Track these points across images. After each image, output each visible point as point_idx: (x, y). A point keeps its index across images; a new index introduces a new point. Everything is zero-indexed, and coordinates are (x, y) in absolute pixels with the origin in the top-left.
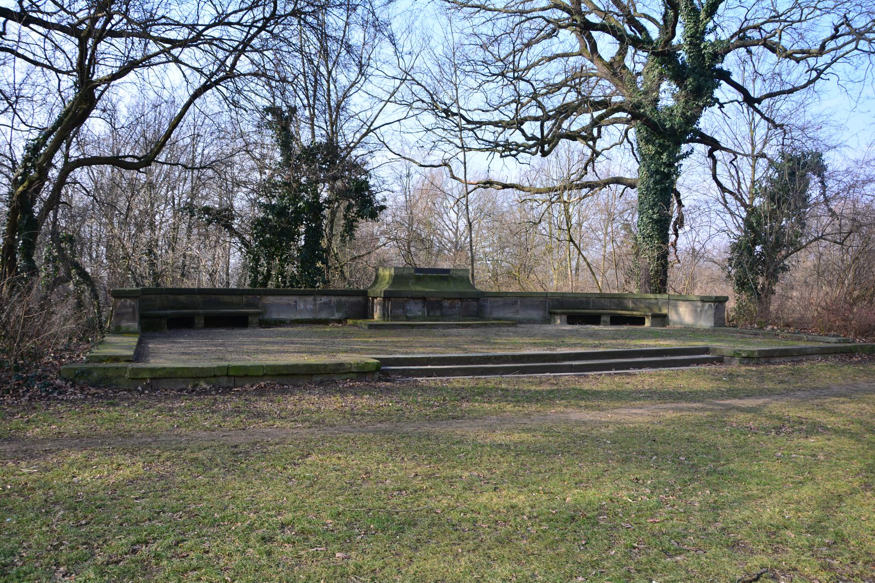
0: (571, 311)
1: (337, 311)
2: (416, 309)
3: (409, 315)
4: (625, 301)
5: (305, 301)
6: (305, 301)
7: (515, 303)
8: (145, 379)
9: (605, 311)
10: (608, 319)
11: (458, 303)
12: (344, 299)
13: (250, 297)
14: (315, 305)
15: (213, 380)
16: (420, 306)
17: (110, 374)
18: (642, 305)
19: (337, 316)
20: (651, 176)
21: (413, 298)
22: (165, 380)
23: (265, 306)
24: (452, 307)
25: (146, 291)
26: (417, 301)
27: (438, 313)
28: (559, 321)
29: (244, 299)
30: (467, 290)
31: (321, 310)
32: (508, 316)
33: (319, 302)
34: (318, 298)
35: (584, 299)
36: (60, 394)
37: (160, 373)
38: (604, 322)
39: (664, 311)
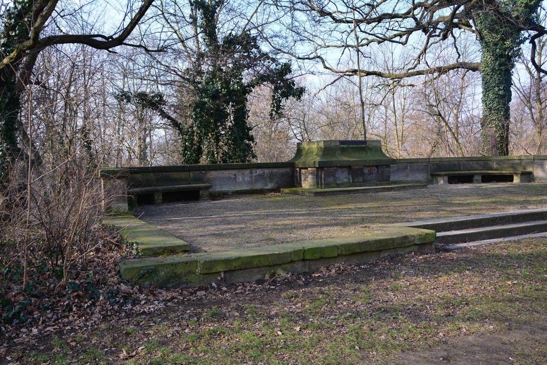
0: (451, 172)
1: (270, 182)
2: (343, 176)
3: (338, 182)
4: (490, 163)
5: (243, 174)
6: (243, 174)
8: (219, 273)
9: (477, 171)
10: (479, 178)
11: (375, 170)
12: (275, 170)
13: (196, 172)
14: (252, 177)
15: (288, 266)
16: (346, 173)
17: (179, 271)
18: (505, 166)
19: (270, 186)
20: (496, 60)
21: (341, 167)
22: (240, 272)
23: (209, 181)
24: (370, 173)
25: (133, 171)
26: (344, 169)
27: (361, 179)
28: (442, 182)
29: (192, 174)
31: (256, 181)
33: (254, 175)
34: (254, 171)
35: (456, 163)
36: (134, 304)
37: (235, 264)
38: (477, 180)
39: (529, 169)
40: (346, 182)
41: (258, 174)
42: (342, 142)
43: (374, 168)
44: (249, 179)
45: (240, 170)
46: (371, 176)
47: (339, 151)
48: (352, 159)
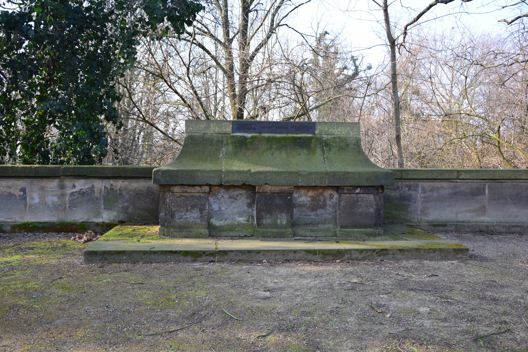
1: (106, 208)
3: (215, 222)
5: (43, 188)
7: (478, 192)
11: (332, 198)
12: (119, 184)
26: (236, 192)
27: (283, 219)
30: (350, 169)
31: (73, 205)
32: (461, 217)
33: (69, 191)
34: (68, 183)
40: (239, 225)
41: (77, 189)
43: (330, 192)
44: (55, 199)
45: (36, 181)
46: (320, 211)
47: (230, 148)
48: (255, 169)
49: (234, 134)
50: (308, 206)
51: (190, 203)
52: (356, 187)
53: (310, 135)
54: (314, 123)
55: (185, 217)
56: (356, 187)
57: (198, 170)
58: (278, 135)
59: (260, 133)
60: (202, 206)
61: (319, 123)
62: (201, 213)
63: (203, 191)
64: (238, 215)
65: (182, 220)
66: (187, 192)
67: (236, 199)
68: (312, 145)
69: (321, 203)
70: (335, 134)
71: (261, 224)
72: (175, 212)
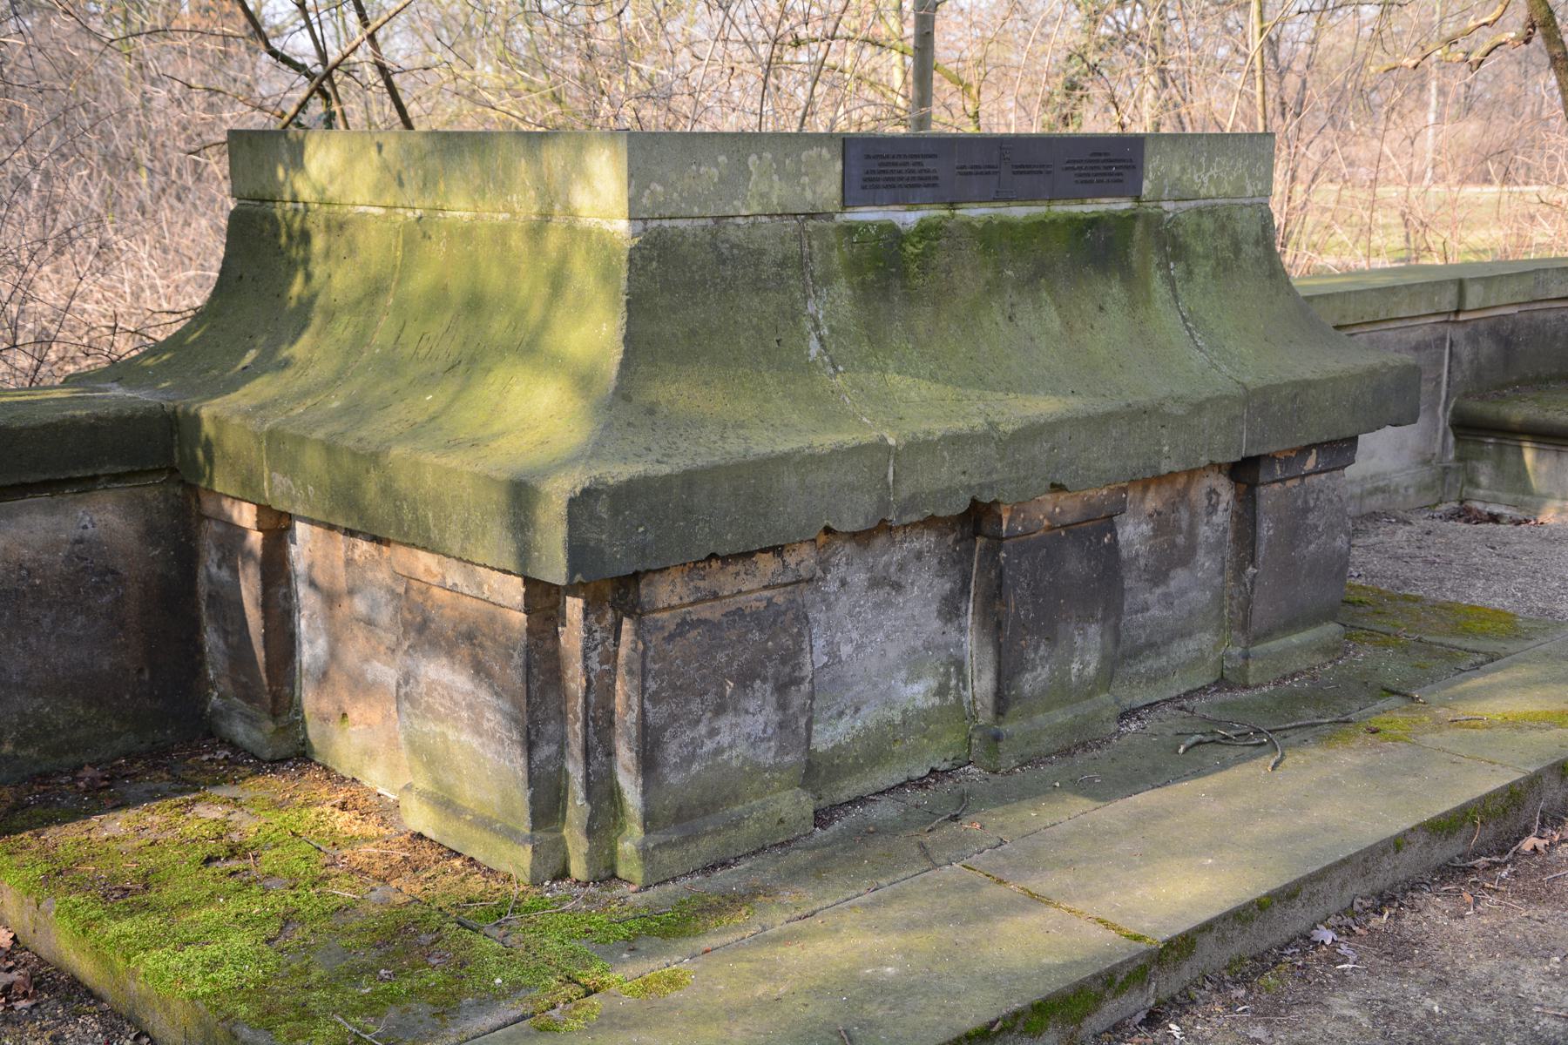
26: (889, 555)
42: (878, 165)
49: (848, 217)
50: (1142, 562)
51: (729, 663)
52: (1305, 451)
53: (1123, 205)
54: (1138, 141)
55: (709, 745)
56: (1305, 451)
57: (784, 458)
58: (1018, 212)
59: (952, 205)
60: (784, 662)
61: (1157, 137)
62: (782, 706)
63: (790, 577)
64: (903, 674)
65: (695, 767)
66: (715, 596)
67: (898, 587)
68: (1135, 257)
69: (1180, 540)
70: (1203, 192)
71: (1017, 698)
72: (664, 729)
